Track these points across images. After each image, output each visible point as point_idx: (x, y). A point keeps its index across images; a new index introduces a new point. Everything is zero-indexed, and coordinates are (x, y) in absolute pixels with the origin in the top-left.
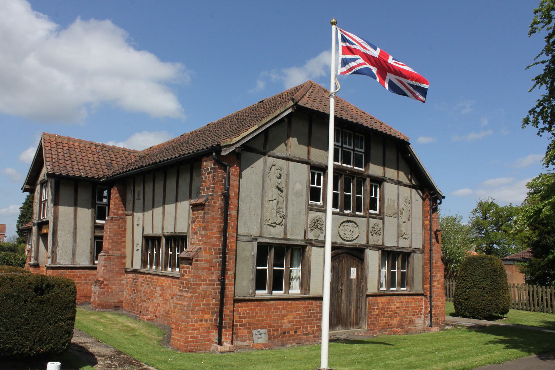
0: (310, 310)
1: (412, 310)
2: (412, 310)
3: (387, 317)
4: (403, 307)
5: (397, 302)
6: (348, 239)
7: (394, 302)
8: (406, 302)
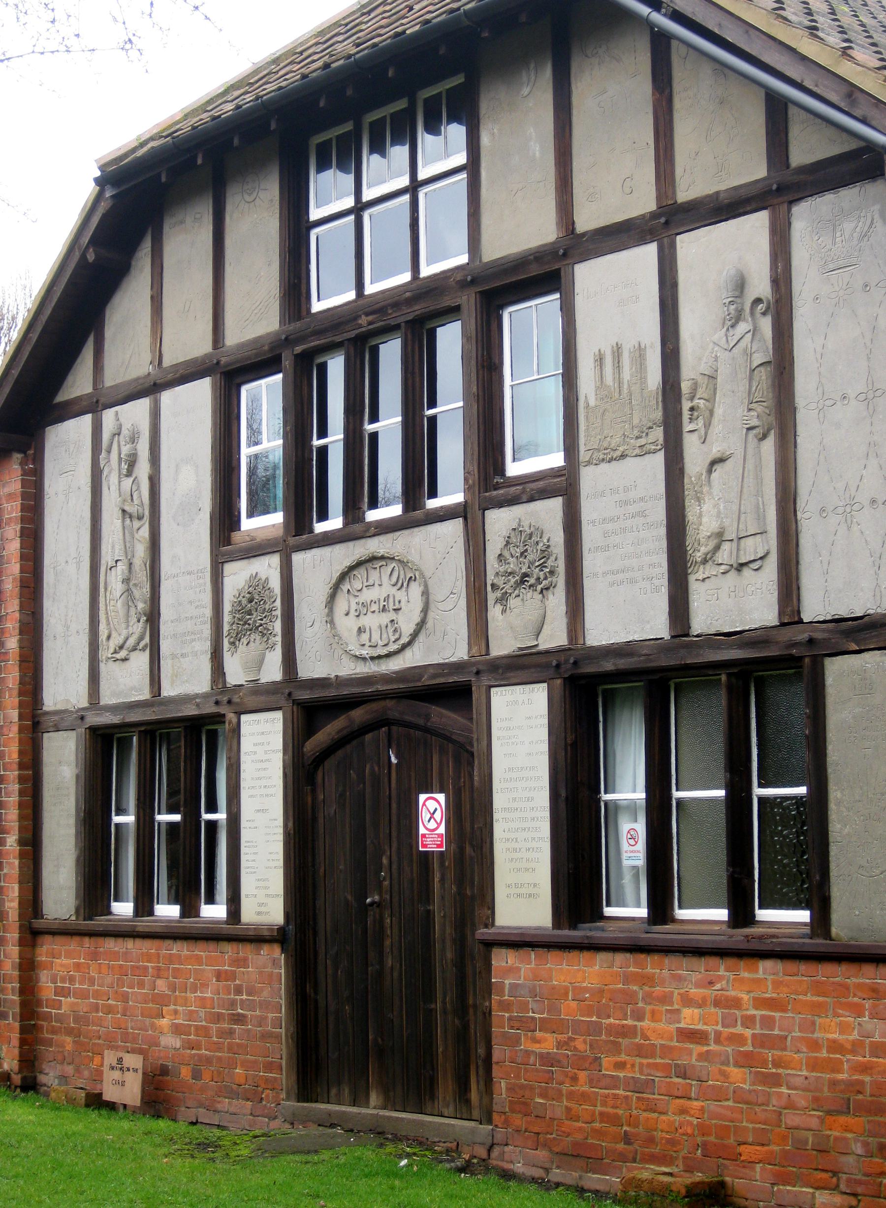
0: (238, 991)
1: (814, 1065)
2: (814, 1065)
3: (614, 1082)
4: (738, 1039)
5: (688, 1001)
6: (384, 651)
7: (665, 999)
8: (760, 1003)
